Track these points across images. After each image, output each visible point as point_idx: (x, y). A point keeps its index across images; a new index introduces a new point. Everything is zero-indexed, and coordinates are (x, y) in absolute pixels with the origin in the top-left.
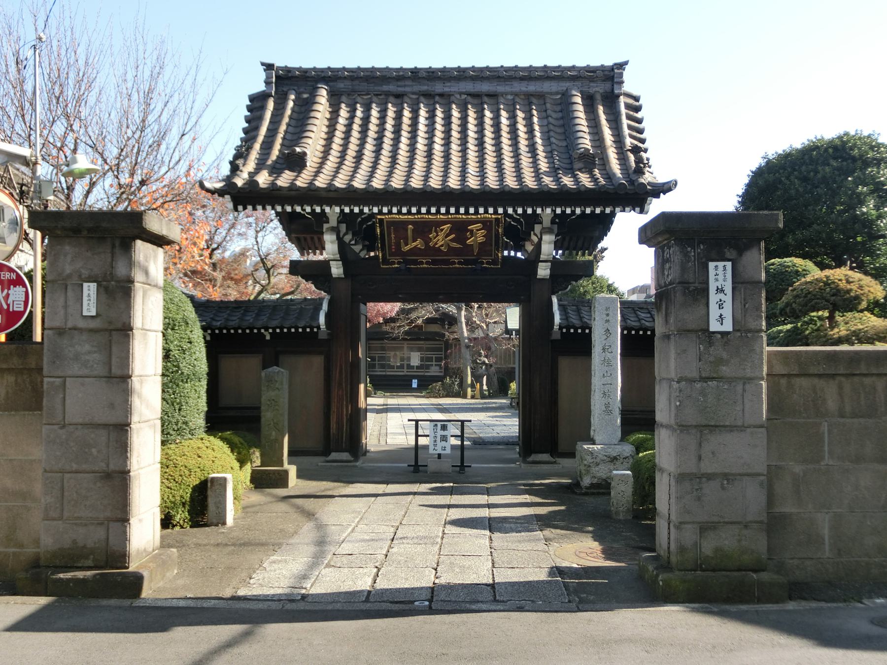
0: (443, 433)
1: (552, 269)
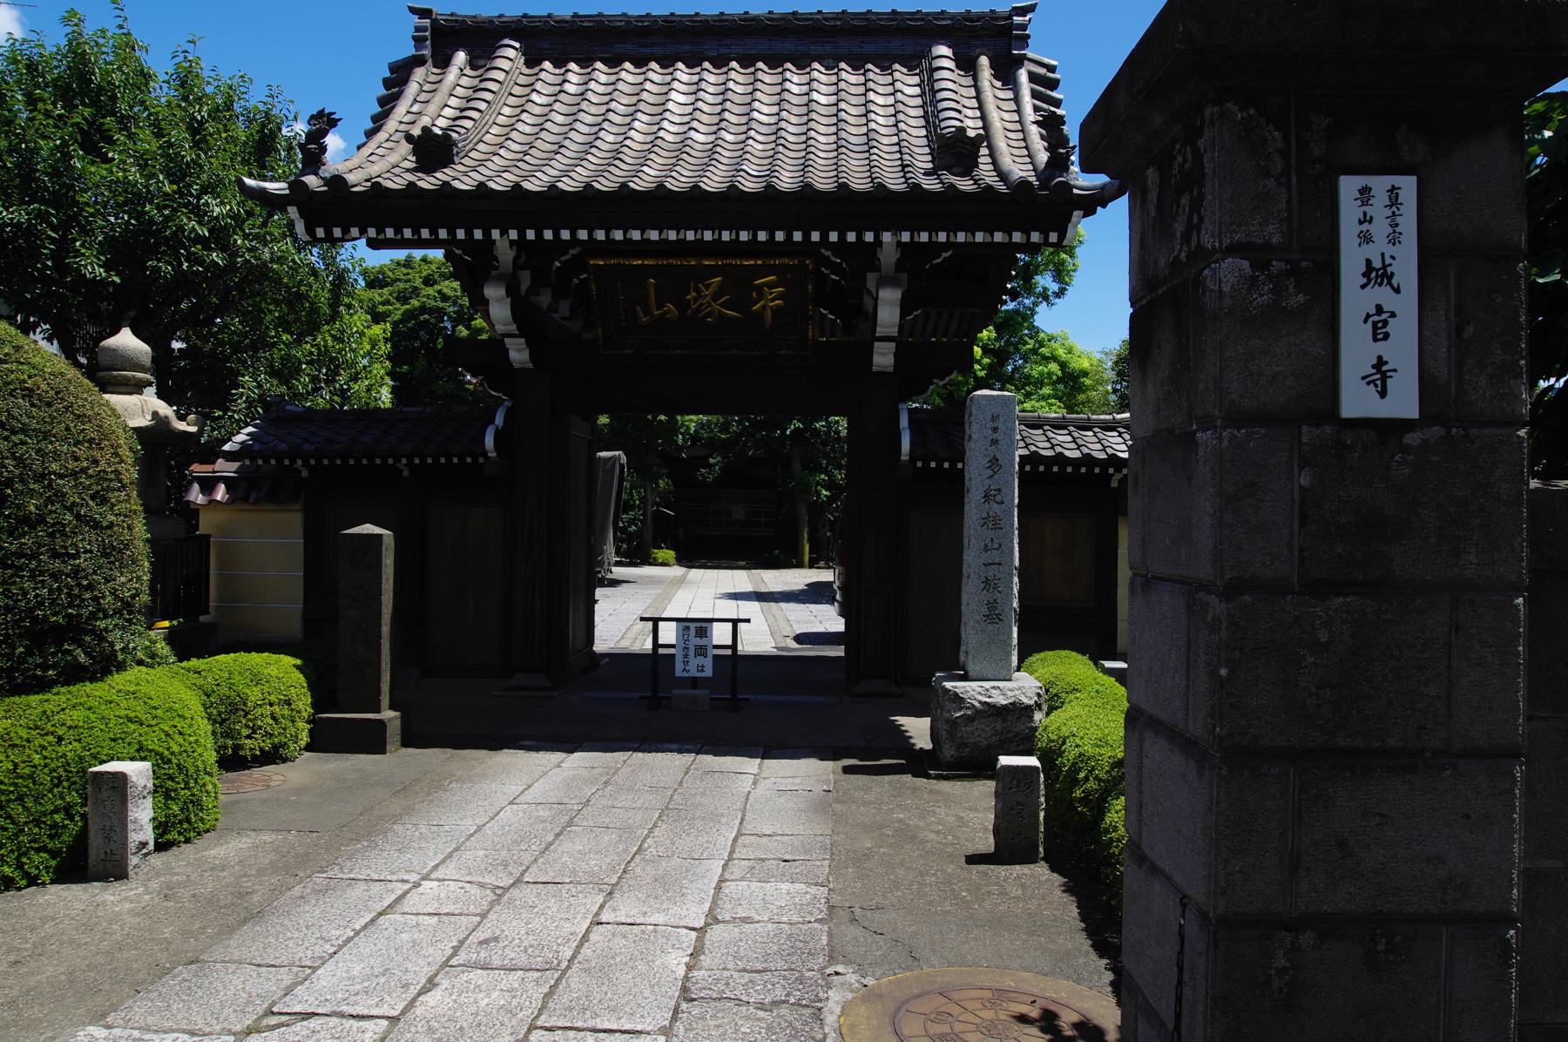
0: (699, 642)
1: (897, 355)
